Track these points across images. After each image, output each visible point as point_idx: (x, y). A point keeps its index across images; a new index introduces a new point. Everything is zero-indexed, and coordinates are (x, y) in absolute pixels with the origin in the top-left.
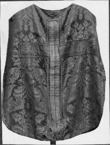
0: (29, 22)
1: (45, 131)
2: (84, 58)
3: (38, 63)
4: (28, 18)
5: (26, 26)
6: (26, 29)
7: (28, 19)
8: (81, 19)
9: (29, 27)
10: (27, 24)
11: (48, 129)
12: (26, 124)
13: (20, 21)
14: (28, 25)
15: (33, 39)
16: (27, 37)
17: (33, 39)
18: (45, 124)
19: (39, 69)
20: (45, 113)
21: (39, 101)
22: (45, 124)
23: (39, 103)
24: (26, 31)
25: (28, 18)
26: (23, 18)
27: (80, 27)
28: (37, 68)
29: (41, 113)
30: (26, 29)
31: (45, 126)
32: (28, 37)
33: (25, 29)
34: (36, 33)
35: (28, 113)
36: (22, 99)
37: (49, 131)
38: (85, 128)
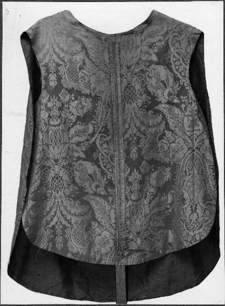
0: (66, 231)
1: (94, 133)
2: (145, 239)
3: (82, 151)
4: (58, 60)
5: (59, 239)
6: (53, 84)
7: (63, 223)
8: (134, 160)
9: (59, 79)
10: (60, 235)
11: (100, 128)
12: (49, 121)
13: (46, 230)
14: (57, 75)
15: (69, 102)
16: (56, 97)
17: (69, 102)
18: (94, 116)
19: (84, 162)
20: (92, 94)
21: (78, 69)
22: (94, 116)
23: (78, 71)
24: (54, 87)
25: (58, 60)
26: (53, 223)
27: (133, 174)
28: (80, 162)
29: (84, 94)
30: (56, 158)
31: (93, 122)
32: (59, 98)
33: (57, 245)
34: (75, 90)
35: (52, 98)
36: (46, 230)
37: (103, 133)
38: (140, 62)
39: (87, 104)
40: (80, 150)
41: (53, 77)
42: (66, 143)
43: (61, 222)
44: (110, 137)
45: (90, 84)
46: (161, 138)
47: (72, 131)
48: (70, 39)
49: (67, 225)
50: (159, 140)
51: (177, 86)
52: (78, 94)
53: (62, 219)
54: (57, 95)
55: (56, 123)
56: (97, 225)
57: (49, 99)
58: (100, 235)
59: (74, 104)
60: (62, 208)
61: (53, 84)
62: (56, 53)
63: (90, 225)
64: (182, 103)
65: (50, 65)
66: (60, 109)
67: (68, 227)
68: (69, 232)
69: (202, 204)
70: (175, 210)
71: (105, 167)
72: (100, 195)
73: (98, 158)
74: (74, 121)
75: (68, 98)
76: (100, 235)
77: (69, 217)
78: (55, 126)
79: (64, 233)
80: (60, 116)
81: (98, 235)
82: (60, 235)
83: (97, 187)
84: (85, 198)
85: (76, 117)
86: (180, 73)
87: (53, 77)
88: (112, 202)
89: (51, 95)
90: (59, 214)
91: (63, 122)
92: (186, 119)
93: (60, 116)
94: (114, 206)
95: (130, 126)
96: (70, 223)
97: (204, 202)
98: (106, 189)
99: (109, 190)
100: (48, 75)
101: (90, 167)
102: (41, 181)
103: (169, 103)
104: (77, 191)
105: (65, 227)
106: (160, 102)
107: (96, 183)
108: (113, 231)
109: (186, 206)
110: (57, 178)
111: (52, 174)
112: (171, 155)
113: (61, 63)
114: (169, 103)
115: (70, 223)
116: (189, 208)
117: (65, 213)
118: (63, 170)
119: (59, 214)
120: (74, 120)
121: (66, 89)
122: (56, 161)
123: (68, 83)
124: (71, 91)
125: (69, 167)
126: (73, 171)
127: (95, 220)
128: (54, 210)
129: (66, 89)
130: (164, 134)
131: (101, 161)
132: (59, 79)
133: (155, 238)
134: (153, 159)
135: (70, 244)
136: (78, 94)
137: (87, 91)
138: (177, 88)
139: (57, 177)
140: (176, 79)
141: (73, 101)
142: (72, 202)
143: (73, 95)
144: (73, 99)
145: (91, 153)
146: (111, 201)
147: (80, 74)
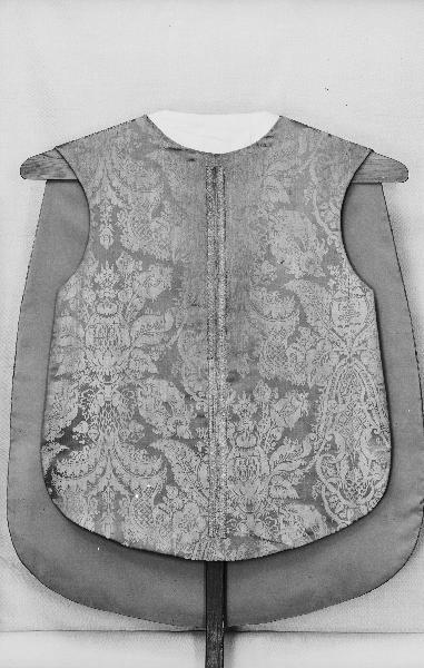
0: (121, 502)
1: (312, 455)
3: (153, 361)
25: (116, 201)
32: (116, 268)
39: (300, 404)
40: (288, 485)
41: (106, 231)
42: (124, 348)
44: (203, 334)
47: (138, 325)
50: (153, 216)
51: (322, 248)
52: (146, 259)
54: (112, 262)
55: (108, 311)
56: (176, 493)
57: (236, 399)
58: (182, 510)
59: (141, 278)
60: (116, 463)
61: (106, 243)
64: (330, 276)
66: (118, 286)
67: (125, 496)
69: (367, 453)
70: (179, 346)
71: (333, 510)
72: (182, 440)
73: (320, 496)
74: (140, 307)
75: (131, 268)
76: (182, 510)
77: (126, 478)
78: (104, 316)
80: (117, 298)
81: (178, 510)
83: (178, 423)
85: (281, 429)
86: (328, 223)
87: (106, 231)
88: (203, 450)
89: (102, 262)
90: (109, 471)
91: (259, 442)
92: (336, 304)
93: (117, 298)
94: (205, 458)
95: (101, 184)
97: (371, 451)
98: (192, 427)
99: (199, 430)
101: (165, 390)
103: (306, 277)
105: (119, 496)
106: (292, 277)
107: (175, 418)
108: (204, 502)
109: (340, 457)
110: (108, 409)
112: (309, 369)
114: (306, 277)
116: (345, 463)
117: (120, 470)
118: (119, 394)
119: (109, 471)
120: (279, 436)
121: (266, 381)
122: (108, 378)
123: (132, 240)
124: (138, 255)
125: (128, 391)
126: (279, 525)
128: (102, 464)
129: (266, 381)
131: (325, 501)
132: (117, 232)
133: (281, 518)
134: (276, 378)
136: (146, 259)
137: (164, 255)
138: (321, 251)
139: (108, 407)
140: (322, 236)
141: (278, 400)
143: (277, 389)
145: (165, 369)
146: (200, 450)
147: (154, 225)
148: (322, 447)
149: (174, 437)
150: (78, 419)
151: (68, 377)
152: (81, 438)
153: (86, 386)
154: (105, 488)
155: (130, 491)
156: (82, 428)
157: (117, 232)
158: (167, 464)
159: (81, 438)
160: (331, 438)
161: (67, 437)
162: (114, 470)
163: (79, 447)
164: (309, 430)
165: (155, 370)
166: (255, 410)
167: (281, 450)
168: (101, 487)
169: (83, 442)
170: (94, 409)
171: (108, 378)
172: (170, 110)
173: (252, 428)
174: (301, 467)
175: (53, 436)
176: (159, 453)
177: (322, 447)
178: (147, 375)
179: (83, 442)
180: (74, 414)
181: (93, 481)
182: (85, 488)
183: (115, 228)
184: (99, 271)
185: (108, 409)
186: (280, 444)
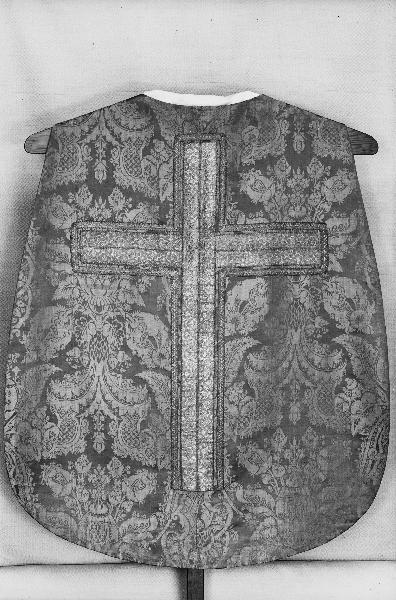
6: (101, 176)
9: (109, 441)
10: (103, 158)
14: (108, 163)
29: (145, 467)
43: (104, 137)
45: (159, 179)
46: (339, 390)
48: (128, 380)
49: (115, 143)
50: (144, 155)
53: (106, 133)
54: (105, 198)
62: (106, 401)
63: (152, 145)
65: (98, 145)
68: (117, 157)
74: (128, 510)
79: (108, 156)
82: (103, 158)
84: (143, 375)
96: (119, 140)
100: (94, 161)
102: (73, 338)
104: (128, 361)
111: (90, 331)
113: (115, 143)
115: (119, 140)
121: (119, 458)
125: (118, 322)
127: (161, 139)
130: (344, 384)
132: (111, 169)
135: (117, 174)
141: (130, 209)
142: (121, 380)
144: (130, 206)
148: (167, 525)
149: (157, 369)
150: (72, 344)
151: (63, 302)
152: (74, 363)
153: (78, 315)
154: (96, 411)
155: (118, 416)
156: (75, 353)
157: (111, 169)
158: (150, 392)
159: (74, 363)
160: (176, 518)
161: (60, 358)
162: (103, 397)
163: (71, 371)
164: (157, 509)
165: (141, 303)
166: (108, 481)
167: (131, 521)
168: (91, 410)
169: (75, 367)
170: (86, 338)
171: (99, 308)
172: (62, 123)
173: (104, 498)
174: (147, 539)
175: (49, 356)
176: (144, 382)
177: (167, 525)
178: (134, 308)
179: (75, 367)
180: (68, 340)
181: (85, 404)
182: (77, 410)
183: (108, 163)
184: (92, 205)
185: (99, 339)
186: (129, 516)
